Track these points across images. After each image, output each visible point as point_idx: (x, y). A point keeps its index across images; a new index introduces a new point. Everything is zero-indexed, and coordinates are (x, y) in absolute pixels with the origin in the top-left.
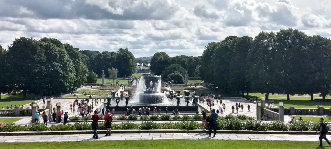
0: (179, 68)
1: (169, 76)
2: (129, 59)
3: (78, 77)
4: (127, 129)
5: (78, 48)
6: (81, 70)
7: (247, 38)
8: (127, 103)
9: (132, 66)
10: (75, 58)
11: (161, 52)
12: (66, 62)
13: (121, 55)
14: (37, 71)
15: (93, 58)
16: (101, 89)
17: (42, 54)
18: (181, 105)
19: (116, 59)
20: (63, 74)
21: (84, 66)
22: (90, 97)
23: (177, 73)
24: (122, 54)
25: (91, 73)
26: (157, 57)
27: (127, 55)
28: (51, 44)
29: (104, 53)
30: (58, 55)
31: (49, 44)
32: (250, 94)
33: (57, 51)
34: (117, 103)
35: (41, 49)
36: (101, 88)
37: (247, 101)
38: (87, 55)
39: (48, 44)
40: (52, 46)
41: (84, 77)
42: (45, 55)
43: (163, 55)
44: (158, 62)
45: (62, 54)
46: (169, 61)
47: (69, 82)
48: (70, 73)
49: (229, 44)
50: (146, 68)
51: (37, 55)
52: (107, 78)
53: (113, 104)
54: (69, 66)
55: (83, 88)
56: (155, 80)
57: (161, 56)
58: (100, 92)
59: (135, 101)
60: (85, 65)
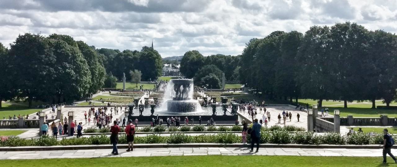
0: (214, 70)
1: (203, 79)
2: (155, 58)
3: (94, 81)
4: (152, 142)
5: (94, 46)
6: (97, 72)
8: (152, 111)
9: (158, 67)
10: (91, 58)
11: (193, 51)
12: (79, 62)
14: (45, 73)
15: (112, 58)
16: (121, 95)
17: (51, 54)
18: (217, 114)
20: (76, 78)
21: (100, 68)
22: (109, 104)
23: (212, 75)
24: (146, 53)
25: (109, 76)
27: (152, 55)
28: (62, 41)
29: (124, 52)
30: (70, 55)
33: (68, 50)
35: (50, 47)
36: (121, 94)
37: (296, 109)
38: (105, 54)
39: (58, 42)
41: (101, 81)
44: (189, 62)
45: (75, 53)
46: (202, 61)
49: (274, 41)
50: (175, 70)
51: (45, 55)
52: (129, 82)
53: (136, 113)
54: (83, 68)
55: (100, 94)
56: (186, 85)
57: (193, 55)
58: (120, 99)
59: (162, 110)
60: (103, 66)
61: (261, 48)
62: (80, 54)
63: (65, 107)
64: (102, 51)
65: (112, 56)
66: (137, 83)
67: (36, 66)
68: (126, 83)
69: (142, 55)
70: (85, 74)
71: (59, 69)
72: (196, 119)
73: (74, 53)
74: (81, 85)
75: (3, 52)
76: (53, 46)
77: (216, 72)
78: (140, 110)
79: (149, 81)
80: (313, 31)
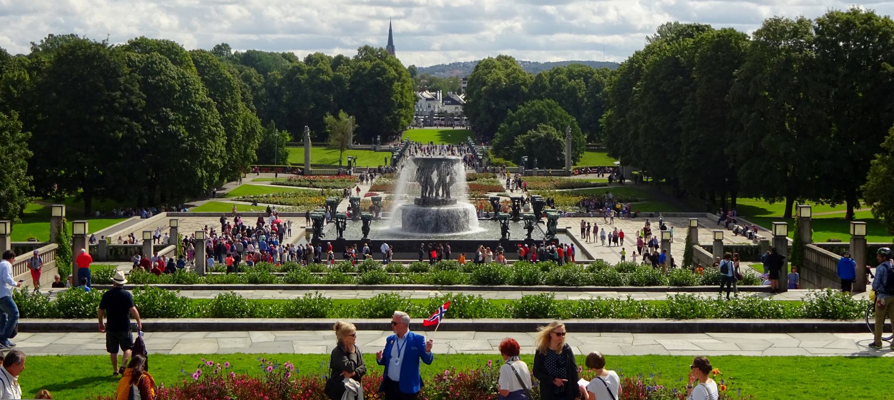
0: (552, 116)
1: (519, 140)
2: (391, 82)
3: (231, 151)
4: (335, 283)
5: (227, 45)
6: (240, 129)
7: (731, 35)
8: (366, 230)
9: (401, 106)
10: (223, 95)
11: (500, 58)
12: (197, 107)
13: (366, 68)
14: (121, 135)
15: (275, 79)
16: (299, 186)
18: (512, 238)
19: (350, 81)
20: (192, 145)
21: (247, 115)
22: (269, 210)
23: (545, 129)
24: (368, 65)
25: (269, 132)
26: (486, 75)
27: (384, 70)
28: (156, 56)
30: (178, 88)
31: (152, 57)
32: (740, 201)
33: (173, 78)
34: (340, 230)
35: (132, 72)
36: (300, 181)
37: (719, 223)
38: (257, 68)
39: (148, 58)
40: (160, 63)
41: (248, 151)
42: (140, 89)
43: (507, 67)
44: (485, 91)
45: (188, 84)
46: (523, 87)
47: (209, 164)
48: (211, 141)
49: (681, 53)
50: (450, 109)
51: (120, 90)
52: (320, 146)
53: (329, 232)
54: (206, 120)
55: (249, 179)
57: (497, 71)
58: (296, 195)
59: (389, 226)
60: (252, 111)
61: (651, 68)
62: (200, 85)
63: (168, 216)
64: (249, 59)
65: (276, 74)
66: (342, 150)
67: (102, 118)
68: (311, 148)
69: (357, 71)
70: (211, 135)
71: (152, 124)
72: (470, 247)
73: (185, 83)
74: (201, 162)
75: (24, 84)
76: (138, 67)
77: (557, 120)
78: (338, 227)
79: (376, 142)
80: (769, 30)
